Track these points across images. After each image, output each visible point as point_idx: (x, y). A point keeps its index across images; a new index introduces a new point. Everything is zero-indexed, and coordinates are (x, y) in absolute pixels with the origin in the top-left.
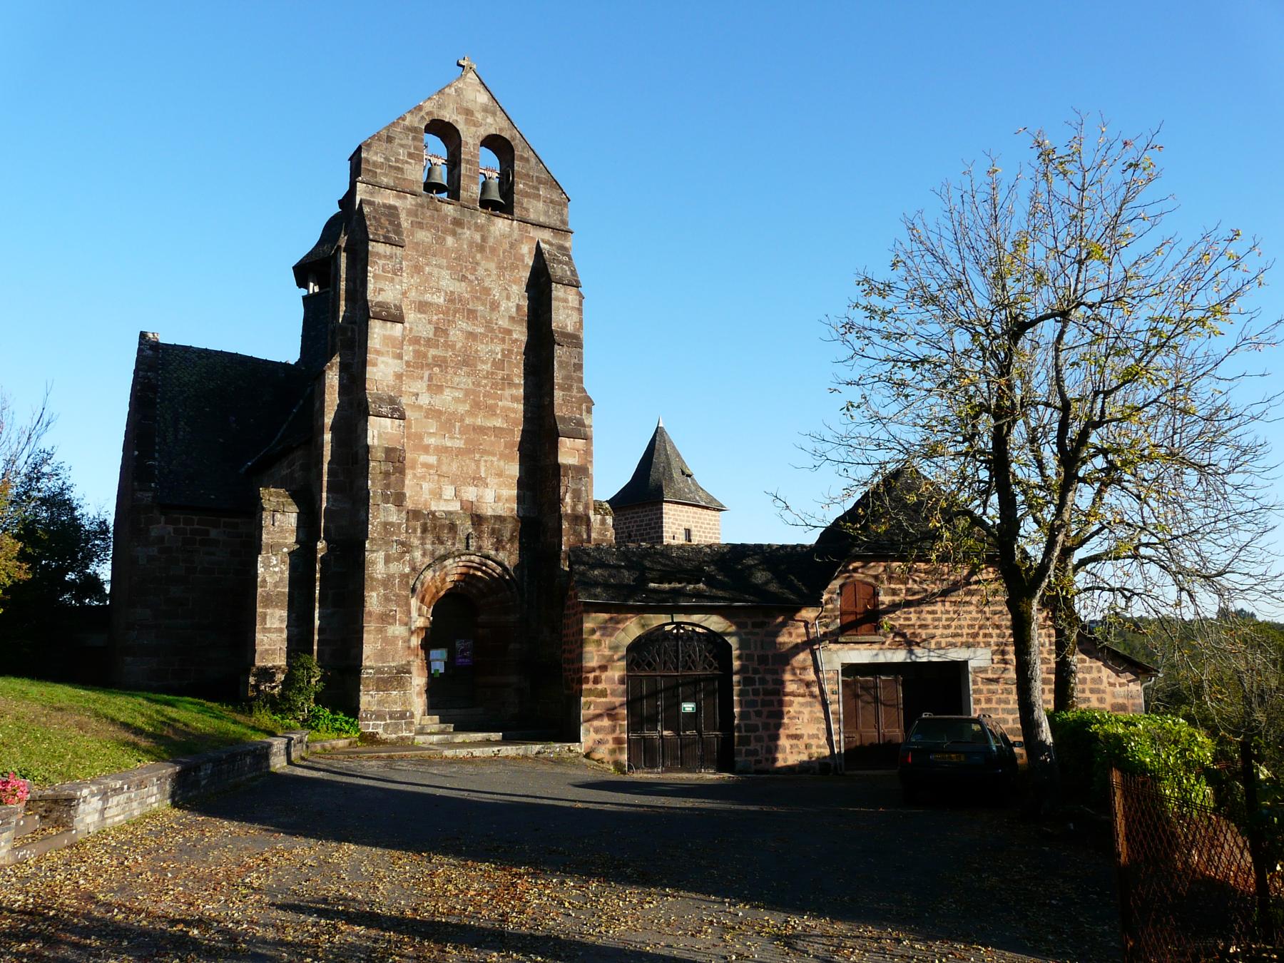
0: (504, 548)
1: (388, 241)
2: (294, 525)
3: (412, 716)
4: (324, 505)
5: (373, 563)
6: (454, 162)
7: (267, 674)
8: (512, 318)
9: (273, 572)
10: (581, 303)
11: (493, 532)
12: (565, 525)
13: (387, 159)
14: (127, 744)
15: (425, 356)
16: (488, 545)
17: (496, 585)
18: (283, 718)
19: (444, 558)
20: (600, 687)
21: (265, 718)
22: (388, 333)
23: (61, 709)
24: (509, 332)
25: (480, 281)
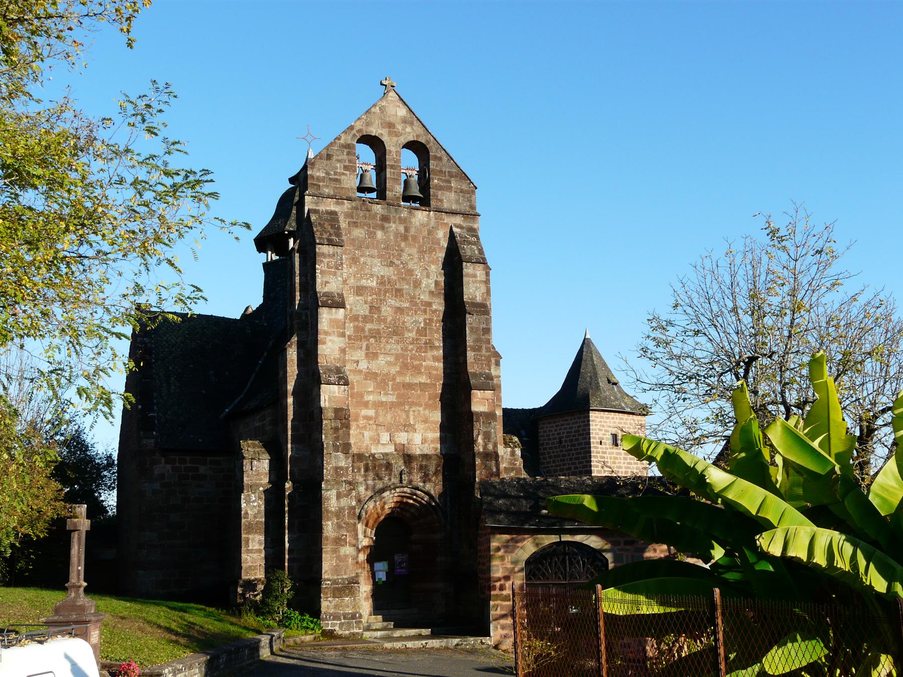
0: (430, 480)
1: (331, 243)
2: (267, 469)
3: (361, 616)
4: (289, 454)
5: (328, 499)
6: (380, 167)
7: (250, 585)
8: (431, 293)
9: (252, 506)
10: (487, 274)
11: (421, 468)
12: (478, 461)
13: (328, 173)
14: (172, 641)
15: (363, 330)
16: (417, 479)
17: (425, 510)
18: (264, 619)
19: (383, 490)
20: (504, 593)
21: (251, 619)
22: (333, 317)
23: (123, 618)
24: (429, 304)
25: (405, 264)
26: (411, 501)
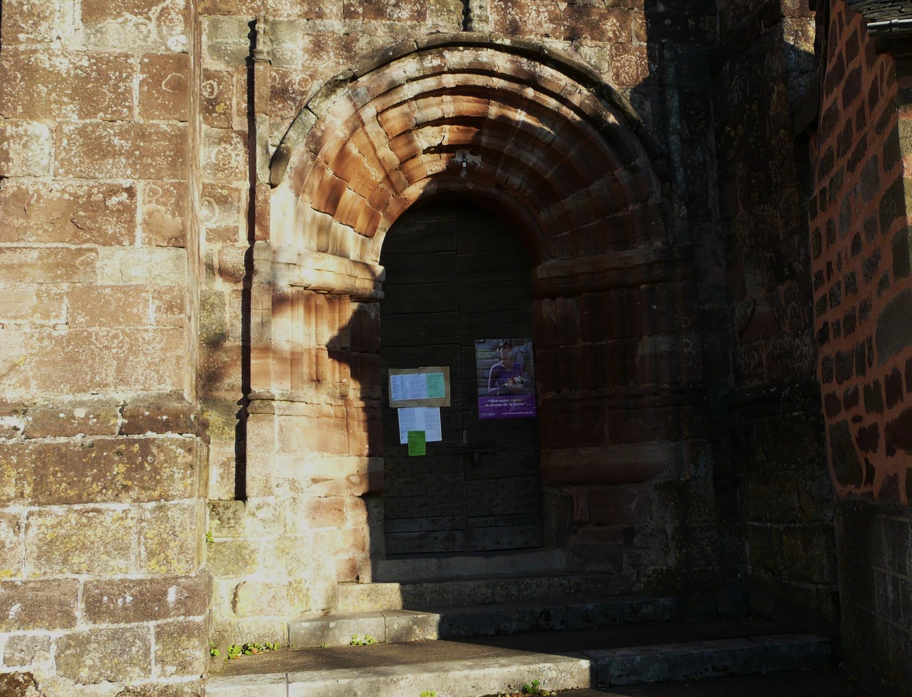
0: (597, 33)
19: (384, 59)
26: (520, 116)
